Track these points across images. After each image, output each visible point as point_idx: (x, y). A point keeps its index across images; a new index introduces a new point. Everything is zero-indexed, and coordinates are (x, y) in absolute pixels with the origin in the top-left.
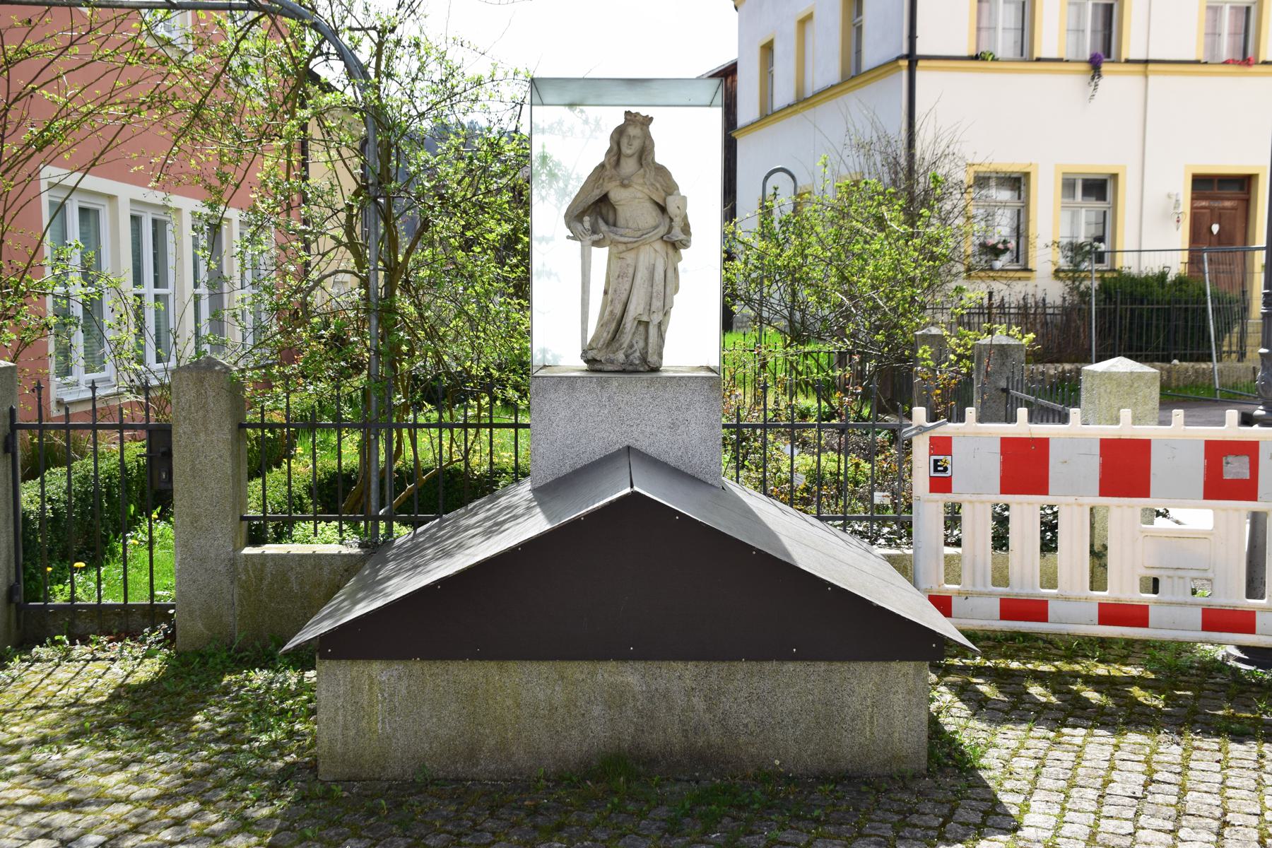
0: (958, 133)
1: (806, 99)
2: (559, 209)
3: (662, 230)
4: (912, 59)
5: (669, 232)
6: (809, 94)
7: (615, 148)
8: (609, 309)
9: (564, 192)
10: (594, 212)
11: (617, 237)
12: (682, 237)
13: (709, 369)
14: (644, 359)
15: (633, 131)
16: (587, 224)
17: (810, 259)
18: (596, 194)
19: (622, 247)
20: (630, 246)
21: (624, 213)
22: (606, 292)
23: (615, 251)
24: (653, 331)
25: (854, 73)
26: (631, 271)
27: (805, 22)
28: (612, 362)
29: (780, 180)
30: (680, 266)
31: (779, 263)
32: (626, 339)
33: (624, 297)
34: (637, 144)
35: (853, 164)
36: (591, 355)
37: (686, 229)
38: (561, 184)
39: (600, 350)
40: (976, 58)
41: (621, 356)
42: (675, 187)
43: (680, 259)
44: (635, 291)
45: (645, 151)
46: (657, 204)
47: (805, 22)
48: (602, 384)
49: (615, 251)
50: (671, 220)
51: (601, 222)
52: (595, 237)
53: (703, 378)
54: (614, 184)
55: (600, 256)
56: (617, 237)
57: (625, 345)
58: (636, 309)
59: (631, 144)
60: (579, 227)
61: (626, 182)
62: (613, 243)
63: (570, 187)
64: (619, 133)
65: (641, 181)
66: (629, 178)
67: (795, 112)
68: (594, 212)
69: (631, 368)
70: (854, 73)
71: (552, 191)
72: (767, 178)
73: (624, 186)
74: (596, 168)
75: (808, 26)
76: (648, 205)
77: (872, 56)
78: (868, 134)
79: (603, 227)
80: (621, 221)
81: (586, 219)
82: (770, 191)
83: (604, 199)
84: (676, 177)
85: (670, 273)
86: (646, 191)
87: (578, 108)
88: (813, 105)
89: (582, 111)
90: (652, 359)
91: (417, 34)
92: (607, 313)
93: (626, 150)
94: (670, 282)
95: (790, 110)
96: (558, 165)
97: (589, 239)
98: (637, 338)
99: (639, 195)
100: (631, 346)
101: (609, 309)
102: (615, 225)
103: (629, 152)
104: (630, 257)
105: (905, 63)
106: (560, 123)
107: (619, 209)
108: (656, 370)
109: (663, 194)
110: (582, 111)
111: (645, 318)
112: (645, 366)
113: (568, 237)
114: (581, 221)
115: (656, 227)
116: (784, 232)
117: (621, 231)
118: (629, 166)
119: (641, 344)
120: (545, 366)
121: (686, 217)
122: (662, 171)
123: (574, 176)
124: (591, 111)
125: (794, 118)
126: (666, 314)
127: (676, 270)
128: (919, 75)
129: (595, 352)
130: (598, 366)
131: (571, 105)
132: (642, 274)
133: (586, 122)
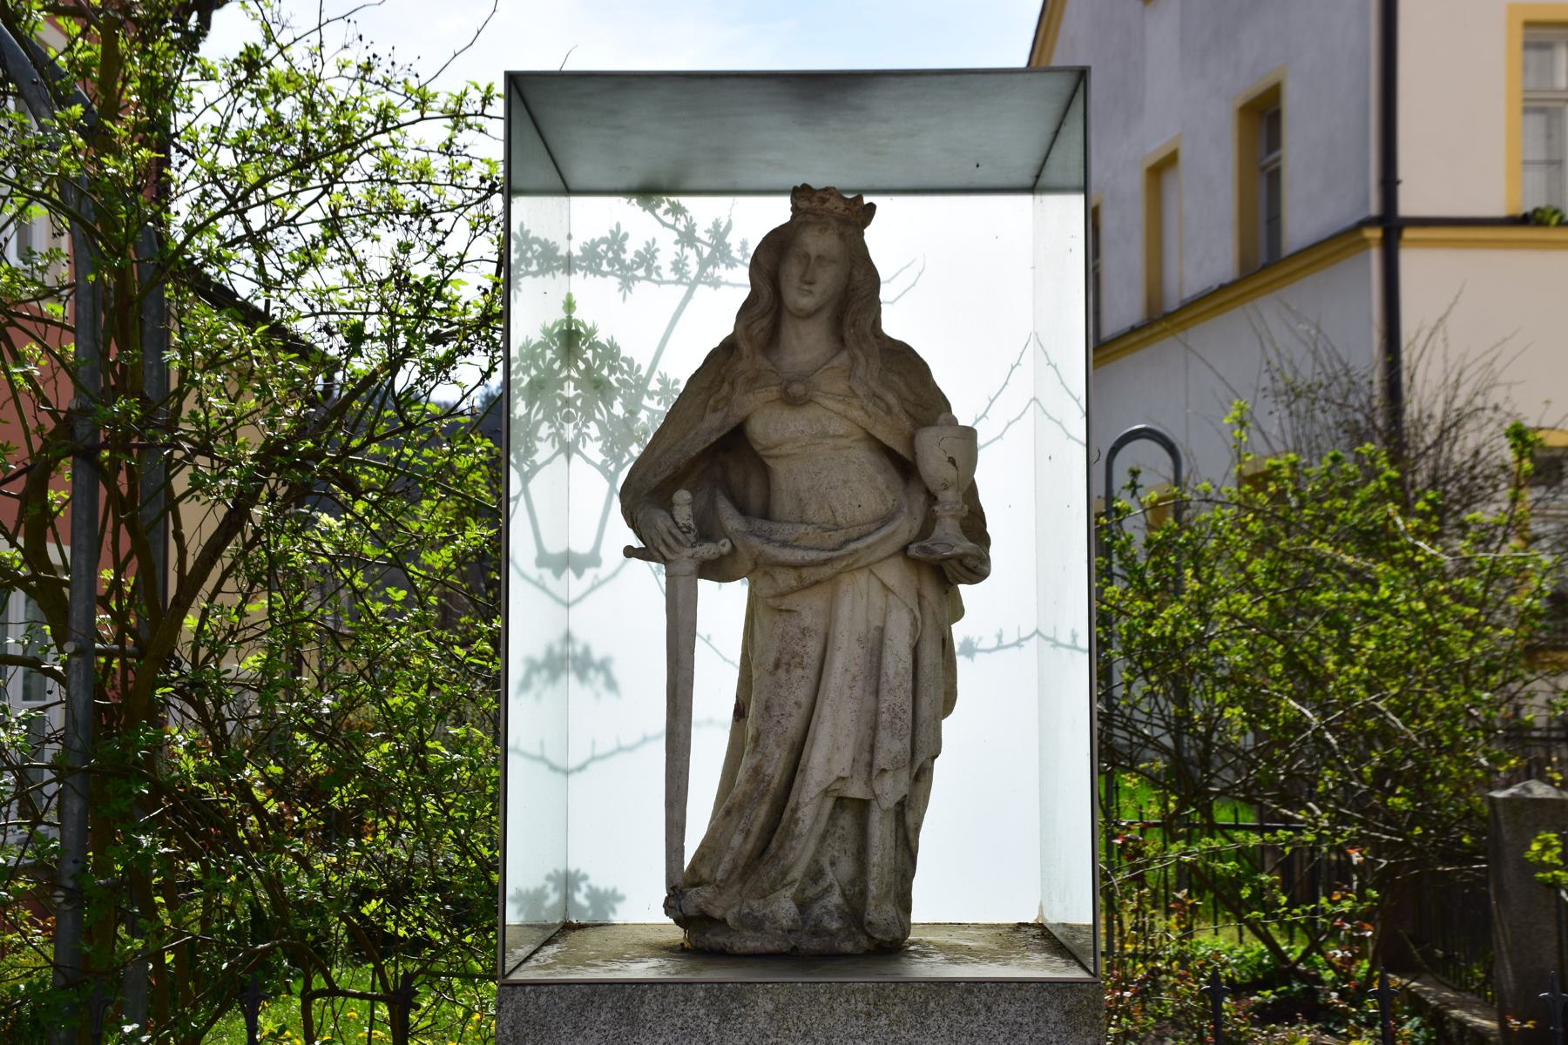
0: (1498, 366)
1: (1168, 316)
2: (612, 478)
3: (904, 528)
4: (1391, 226)
5: (926, 530)
6: (1172, 304)
7: (766, 291)
8: (747, 762)
9: (615, 436)
10: (702, 486)
11: (772, 551)
12: (965, 546)
13: (1047, 938)
14: (854, 913)
15: (817, 242)
16: (684, 514)
17: (1222, 623)
18: (712, 425)
19: (787, 579)
20: (810, 575)
21: (790, 479)
22: (740, 712)
23: (766, 589)
24: (880, 830)
25: (1266, 260)
26: (813, 647)
27: (1161, 170)
28: (756, 924)
29: (1146, 454)
30: (959, 631)
31: (1153, 632)
32: (800, 855)
33: (793, 724)
34: (827, 280)
35: (1275, 441)
36: (696, 899)
37: (975, 525)
38: (618, 409)
39: (721, 887)
40: (1524, 220)
41: (784, 907)
42: (940, 404)
43: (958, 613)
44: (825, 711)
45: (858, 287)
46: (887, 452)
47: (1161, 170)
48: (725, 1002)
49: (766, 589)
50: (932, 498)
51: (726, 511)
52: (708, 550)
53: (1043, 983)
54: (762, 395)
55: (723, 607)
56: (772, 551)
57: (797, 873)
58: (830, 758)
59: (815, 286)
60: (661, 521)
61: (797, 389)
62: (758, 570)
63: (643, 416)
64: (774, 254)
65: (841, 386)
66: (804, 378)
67: (1144, 342)
68: (702, 486)
69: (815, 944)
70: (1266, 260)
71: (593, 430)
72: (1114, 451)
73: (792, 401)
74: (713, 355)
75: (1169, 181)
76: (862, 455)
77: (1303, 222)
78: (1308, 373)
79: (732, 521)
80: (784, 503)
81: (682, 496)
82: (1121, 478)
83: (736, 441)
84: (942, 378)
85: (930, 654)
86: (856, 414)
87: (666, 203)
88: (1183, 326)
89: (677, 210)
90: (879, 913)
91: (258, 38)
92: (742, 775)
93: (797, 298)
94: (932, 684)
95: (1134, 339)
96: (610, 353)
97: (686, 558)
98: (834, 849)
99: (837, 426)
100: (815, 874)
101: (747, 762)
102: (766, 514)
103: (807, 302)
104: (809, 608)
105: (1375, 234)
106: (617, 241)
107: (779, 468)
108: (892, 945)
109: (907, 424)
110: (677, 210)
111: (856, 790)
112: (864, 933)
113: (629, 552)
114: (668, 506)
115: (886, 519)
116: (1156, 567)
117: (785, 531)
118: (806, 344)
119: (846, 868)
120: (568, 927)
121: (971, 492)
122: (905, 364)
123: (654, 385)
124: (703, 210)
125: (1142, 354)
126: (921, 776)
127: (946, 643)
128: (1409, 260)
129: (707, 892)
130: (717, 939)
131: (647, 192)
132: (846, 659)
133: (688, 238)
